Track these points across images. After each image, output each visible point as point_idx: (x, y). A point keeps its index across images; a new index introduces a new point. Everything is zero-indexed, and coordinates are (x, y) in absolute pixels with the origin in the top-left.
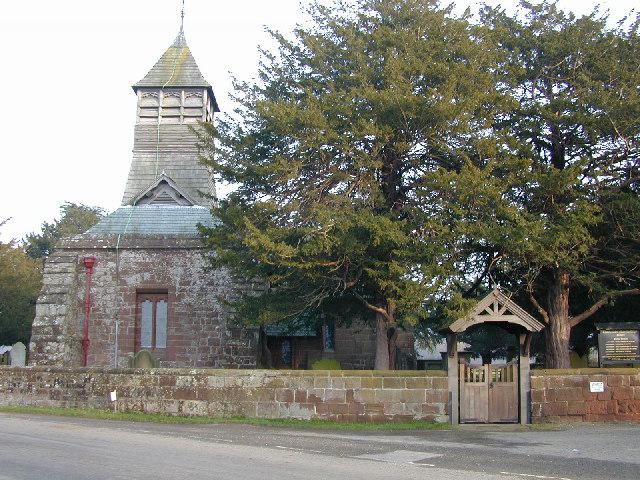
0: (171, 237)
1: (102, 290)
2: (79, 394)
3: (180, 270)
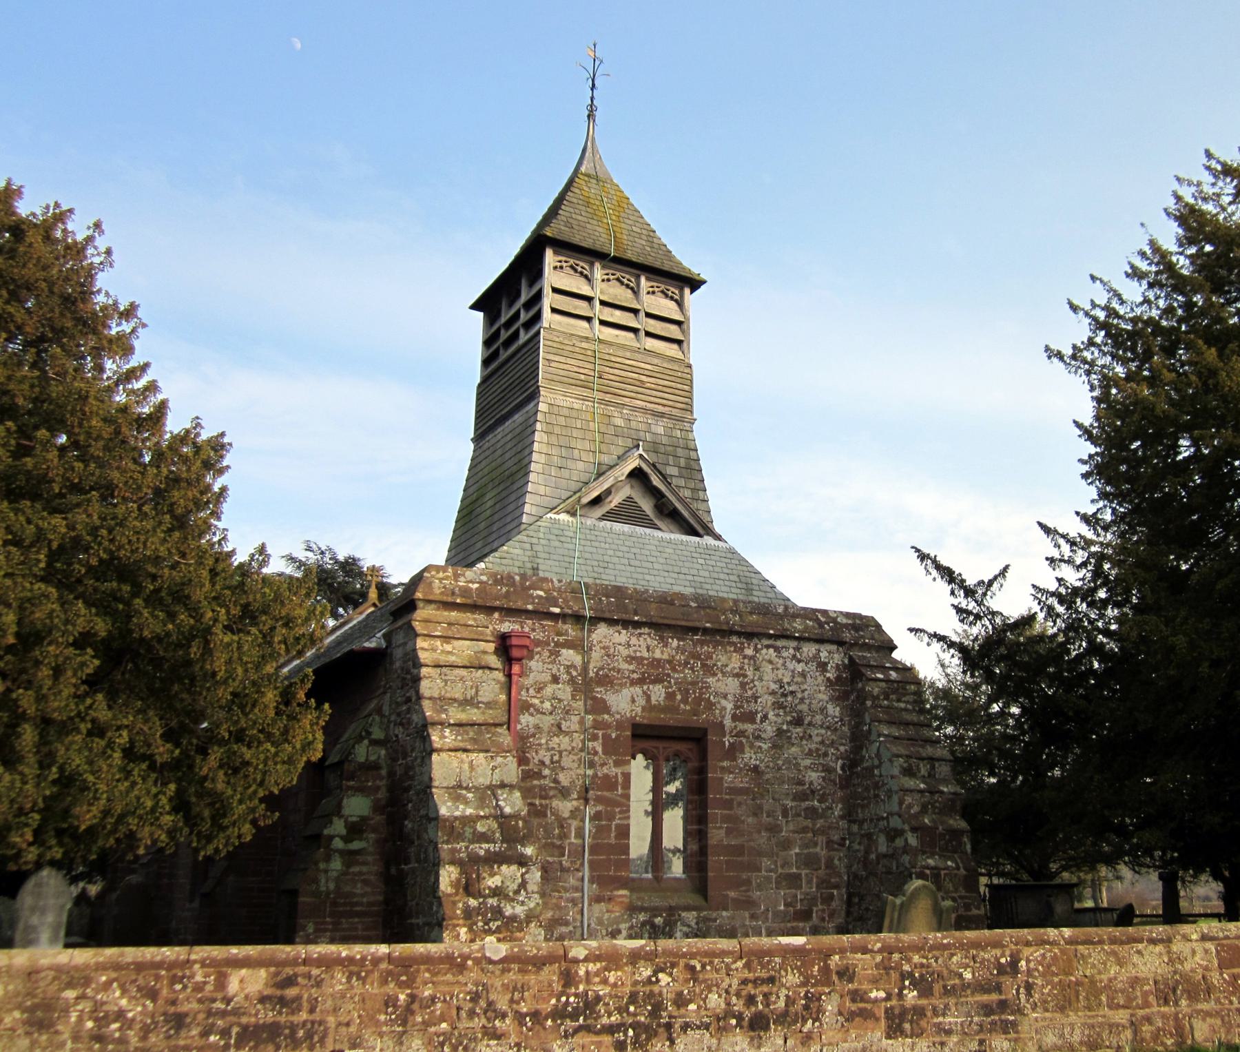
1: (547, 721)
2: (987, 1010)
3: (732, 685)
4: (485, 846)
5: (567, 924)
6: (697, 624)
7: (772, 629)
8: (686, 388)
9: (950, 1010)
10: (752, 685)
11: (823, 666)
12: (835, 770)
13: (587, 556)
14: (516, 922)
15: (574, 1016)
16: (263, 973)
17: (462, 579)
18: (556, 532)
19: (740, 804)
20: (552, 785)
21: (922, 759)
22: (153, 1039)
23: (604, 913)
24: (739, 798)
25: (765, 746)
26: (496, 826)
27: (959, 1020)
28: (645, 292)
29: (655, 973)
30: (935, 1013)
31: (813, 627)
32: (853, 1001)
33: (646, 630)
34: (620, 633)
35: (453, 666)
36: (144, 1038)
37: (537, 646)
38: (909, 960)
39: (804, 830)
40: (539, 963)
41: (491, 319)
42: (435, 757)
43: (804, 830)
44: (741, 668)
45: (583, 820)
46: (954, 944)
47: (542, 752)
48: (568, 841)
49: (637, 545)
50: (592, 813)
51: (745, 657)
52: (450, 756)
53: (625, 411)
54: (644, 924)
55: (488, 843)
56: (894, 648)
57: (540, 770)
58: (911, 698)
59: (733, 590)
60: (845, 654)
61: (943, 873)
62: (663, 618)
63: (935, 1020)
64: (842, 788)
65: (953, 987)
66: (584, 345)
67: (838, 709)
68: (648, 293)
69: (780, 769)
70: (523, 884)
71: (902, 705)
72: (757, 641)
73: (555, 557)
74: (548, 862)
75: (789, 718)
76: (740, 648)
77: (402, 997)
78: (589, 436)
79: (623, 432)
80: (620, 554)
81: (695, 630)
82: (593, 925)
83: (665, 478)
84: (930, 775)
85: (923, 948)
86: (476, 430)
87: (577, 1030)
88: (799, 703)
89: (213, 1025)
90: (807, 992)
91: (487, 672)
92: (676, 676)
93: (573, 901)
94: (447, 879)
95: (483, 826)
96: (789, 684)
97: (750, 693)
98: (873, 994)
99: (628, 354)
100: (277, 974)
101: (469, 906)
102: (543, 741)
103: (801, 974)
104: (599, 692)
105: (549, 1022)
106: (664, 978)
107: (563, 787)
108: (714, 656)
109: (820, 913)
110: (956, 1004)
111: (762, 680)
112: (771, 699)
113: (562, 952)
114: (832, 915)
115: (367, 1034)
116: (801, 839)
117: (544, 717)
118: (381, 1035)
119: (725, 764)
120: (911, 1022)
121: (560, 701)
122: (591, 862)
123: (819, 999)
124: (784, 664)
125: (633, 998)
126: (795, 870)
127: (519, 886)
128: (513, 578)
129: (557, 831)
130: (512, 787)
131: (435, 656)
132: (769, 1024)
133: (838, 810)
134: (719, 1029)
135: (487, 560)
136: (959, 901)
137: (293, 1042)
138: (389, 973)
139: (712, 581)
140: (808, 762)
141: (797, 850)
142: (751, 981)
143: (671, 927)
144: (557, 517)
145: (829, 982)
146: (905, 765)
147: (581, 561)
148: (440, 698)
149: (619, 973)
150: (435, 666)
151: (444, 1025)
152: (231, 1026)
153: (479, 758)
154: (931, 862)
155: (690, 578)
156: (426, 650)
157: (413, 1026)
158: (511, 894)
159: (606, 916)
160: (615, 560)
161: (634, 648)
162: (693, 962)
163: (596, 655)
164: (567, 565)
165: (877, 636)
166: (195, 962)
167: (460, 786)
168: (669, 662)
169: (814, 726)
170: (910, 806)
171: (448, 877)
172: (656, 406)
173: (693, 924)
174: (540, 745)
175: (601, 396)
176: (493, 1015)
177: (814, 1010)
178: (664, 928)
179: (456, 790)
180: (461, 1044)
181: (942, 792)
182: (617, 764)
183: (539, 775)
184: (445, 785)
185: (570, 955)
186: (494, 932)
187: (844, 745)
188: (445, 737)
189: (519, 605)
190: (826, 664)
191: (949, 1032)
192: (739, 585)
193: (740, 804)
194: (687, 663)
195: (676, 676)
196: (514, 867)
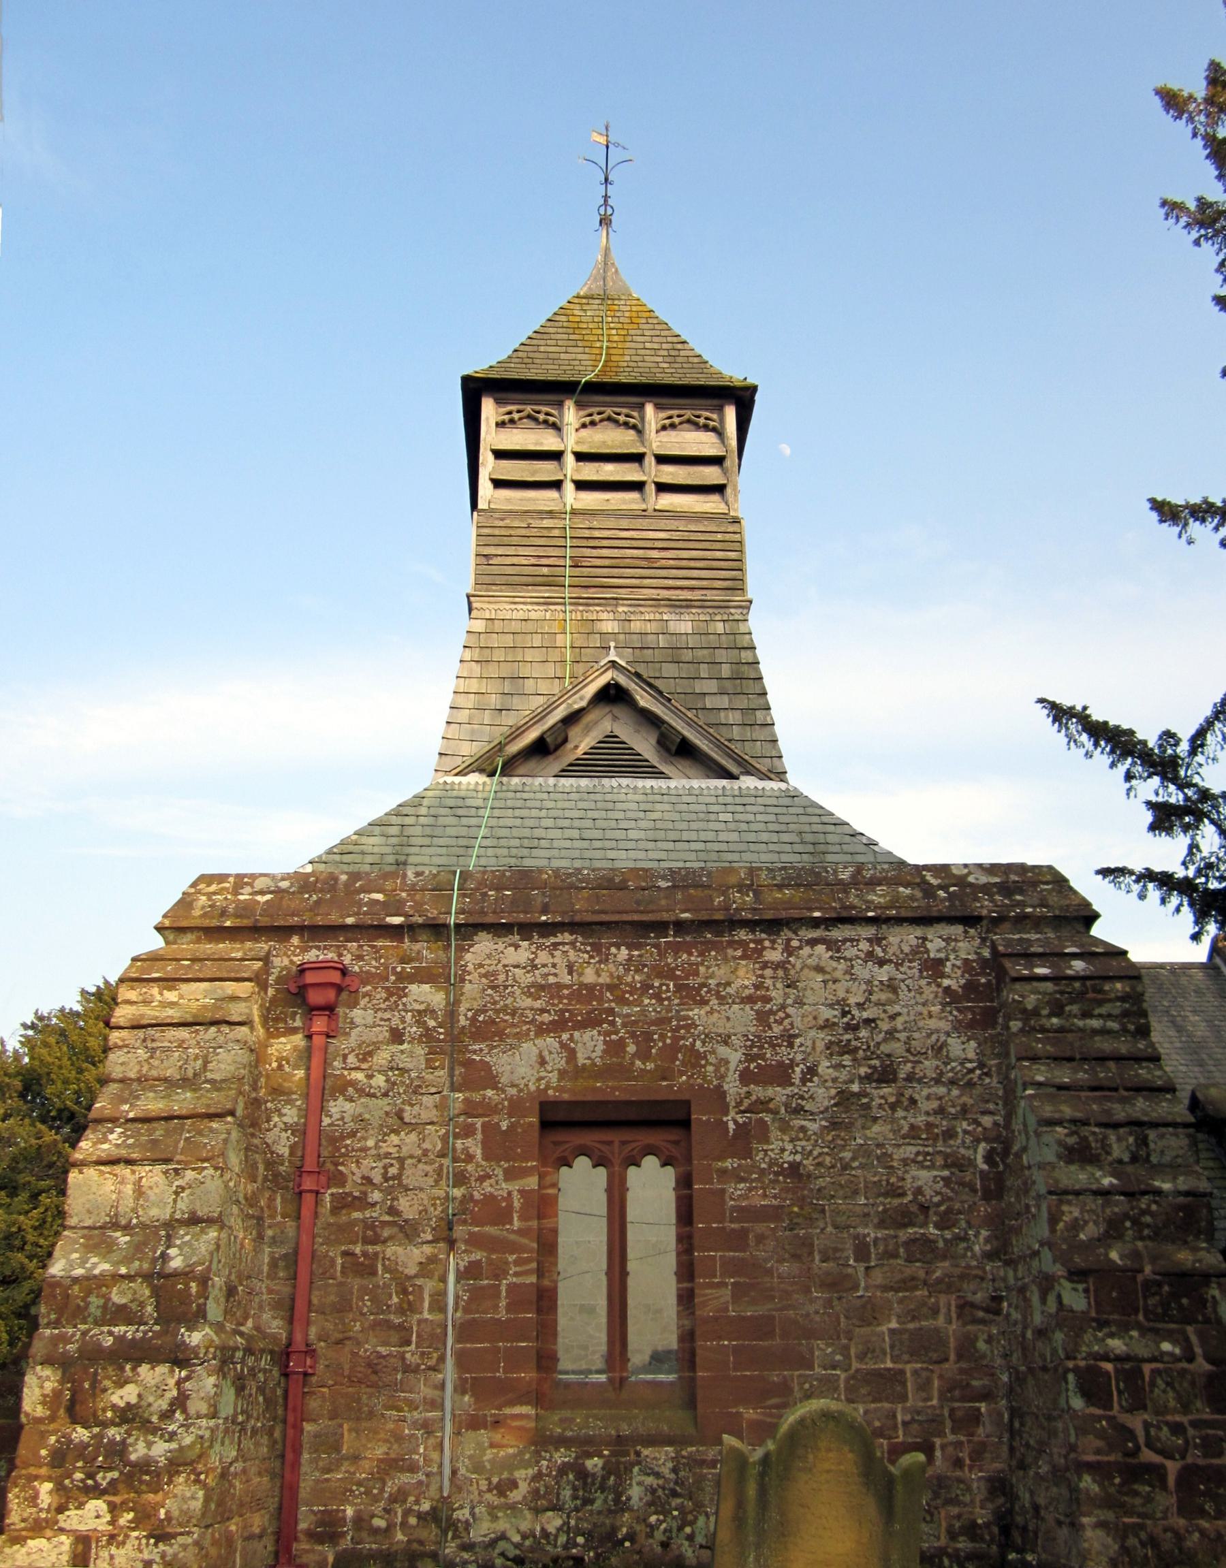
0: (684, 881)
3: (741, 1019)
5: (413, 1468)
6: (665, 916)
8: (732, 555)
10: (781, 1014)
11: (934, 968)
12: (972, 1163)
14: (147, 1473)
18: (451, 803)
19: (760, 1239)
20: (387, 1218)
21: (1116, 1126)
23: (483, 1451)
24: (760, 1228)
25: (813, 1127)
26: (147, 1292)
28: (654, 427)
33: (567, 937)
34: (517, 947)
39: (908, 1284)
42: (73, 1176)
43: (908, 1284)
44: (757, 987)
45: (443, 1279)
47: (367, 1163)
50: (462, 1264)
51: (765, 966)
52: (102, 1173)
53: (620, 609)
54: (563, 1470)
56: (1092, 917)
57: (365, 1194)
58: (1116, 1008)
60: (984, 940)
61: (1147, 1368)
62: (594, 912)
64: (987, 1196)
66: (547, 523)
67: (973, 1044)
69: (846, 1167)
70: (180, 1402)
71: (1095, 1023)
72: (791, 935)
75: (863, 1071)
76: (755, 950)
78: (555, 655)
81: (660, 927)
82: (463, 1471)
84: (1134, 1159)
88: (885, 1040)
92: (626, 1010)
93: (428, 1428)
95: (122, 1293)
96: (860, 1006)
97: (777, 1029)
99: (624, 523)
102: (370, 1143)
104: (478, 1051)
108: (702, 969)
109: (950, 1449)
111: (802, 1004)
112: (822, 1037)
114: (978, 1453)
116: (901, 1301)
117: (372, 1102)
119: (728, 1164)
121: (403, 1071)
124: (849, 972)
126: (889, 1365)
127: (171, 1404)
129: (395, 1300)
133: (980, 1242)
136: (1191, 1432)
140: (909, 1151)
141: (894, 1325)
146: (1072, 1140)
148: (139, 1080)
150: (133, 1027)
153: (153, 1176)
154: (1117, 1345)
155: (700, 846)
158: (155, 1419)
159: (489, 1454)
160: (557, 834)
161: (545, 970)
163: (471, 988)
164: (461, 851)
165: (1053, 899)
168: (611, 987)
169: (919, 1081)
170: (1075, 1226)
173: (666, 1471)
174: (365, 1149)
175: (577, 592)
178: (605, 1479)
181: (1158, 1192)
182: (510, 1175)
183: (362, 1202)
187: (991, 1113)
189: (334, 918)
190: (940, 962)
193: (760, 1239)
194: (646, 987)
196: (162, 1369)
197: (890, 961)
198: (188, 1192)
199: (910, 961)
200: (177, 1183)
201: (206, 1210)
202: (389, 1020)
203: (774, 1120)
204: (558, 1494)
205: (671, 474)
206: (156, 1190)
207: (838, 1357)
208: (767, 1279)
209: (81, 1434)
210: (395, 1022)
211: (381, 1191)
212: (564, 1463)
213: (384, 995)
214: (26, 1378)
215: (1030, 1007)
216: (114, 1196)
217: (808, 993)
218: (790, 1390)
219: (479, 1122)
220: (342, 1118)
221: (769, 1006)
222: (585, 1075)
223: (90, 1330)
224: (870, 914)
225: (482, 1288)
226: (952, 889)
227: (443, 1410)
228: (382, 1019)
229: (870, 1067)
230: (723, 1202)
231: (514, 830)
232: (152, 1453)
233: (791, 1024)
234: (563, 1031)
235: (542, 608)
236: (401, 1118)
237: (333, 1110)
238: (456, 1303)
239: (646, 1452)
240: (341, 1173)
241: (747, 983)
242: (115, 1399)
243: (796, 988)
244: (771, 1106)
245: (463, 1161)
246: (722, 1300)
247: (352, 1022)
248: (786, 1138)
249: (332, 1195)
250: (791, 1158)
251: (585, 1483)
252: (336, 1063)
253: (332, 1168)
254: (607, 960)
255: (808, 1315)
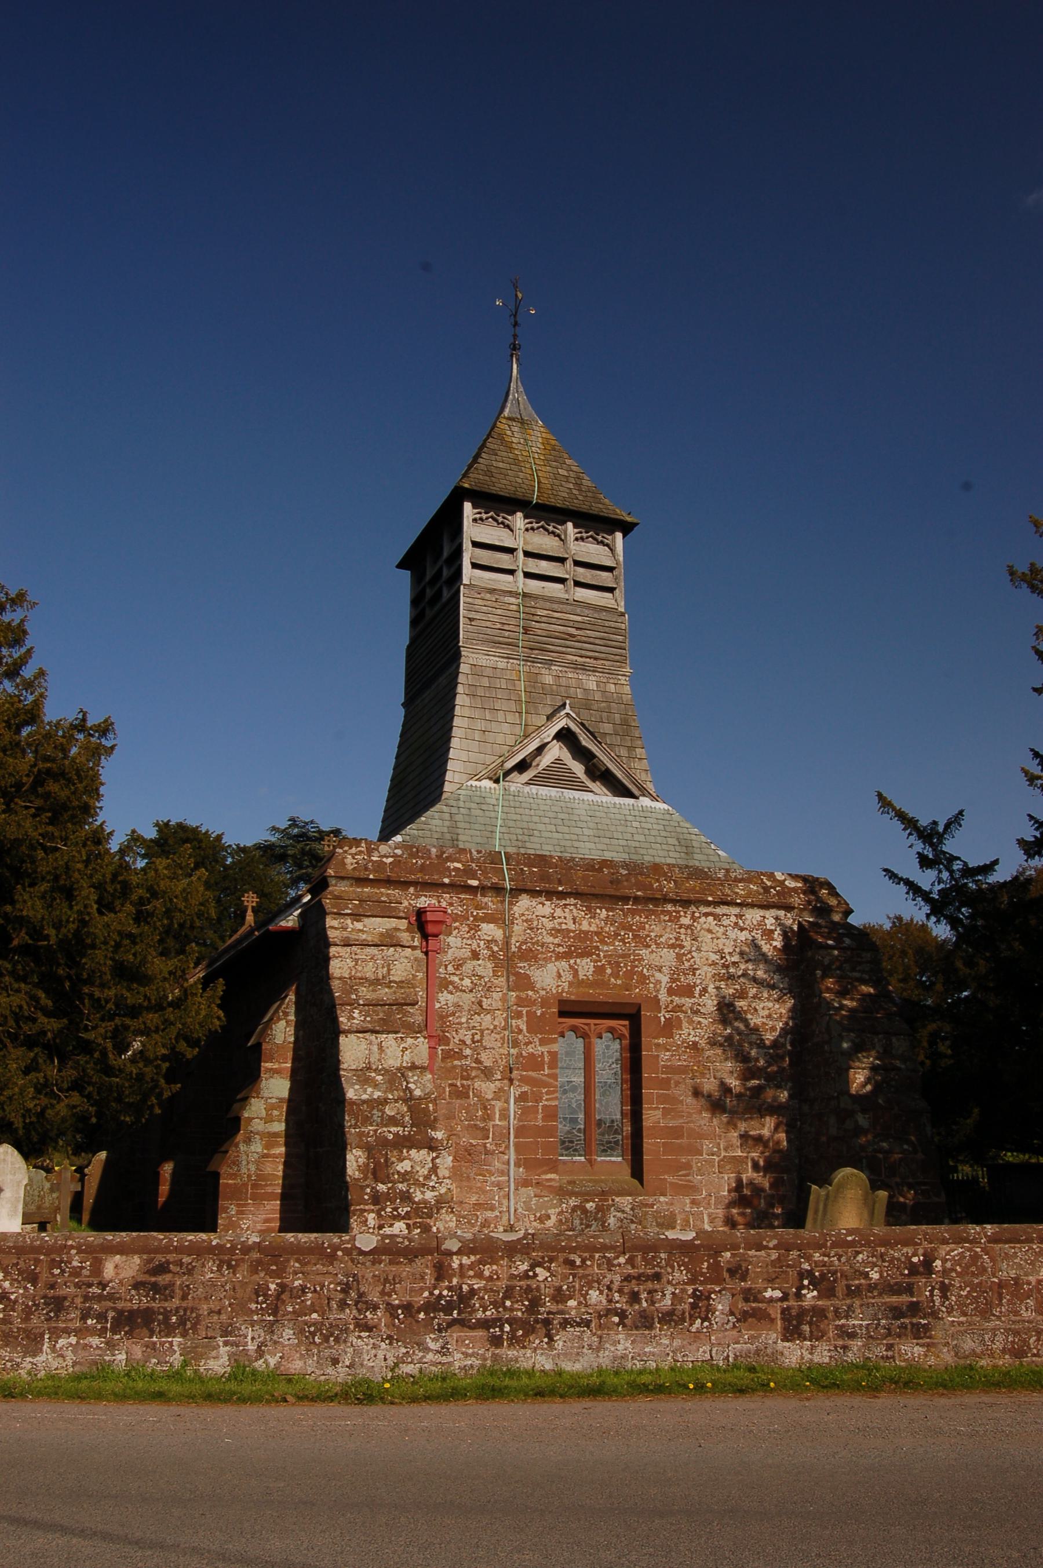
0: (634, 868)
1: (467, 999)
2: (896, 1312)
3: (668, 957)
4: (393, 1129)
5: (492, 1209)
7: (711, 895)
9: (854, 1312)
10: (689, 956)
13: (512, 823)
15: (448, 1309)
16: (137, 1260)
17: (376, 853)
20: (474, 1065)
22: (34, 1320)
24: (676, 1077)
26: (405, 1109)
27: (864, 1323)
28: (573, 538)
29: (532, 1267)
30: (837, 1315)
31: (757, 891)
32: (746, 1300)
33: (573, 901)
34: (544, 905)
35: (365, 944)
36: (27, 1319)
37: (455, 921)
38: (808, 1258)
40: (411, 1254)
41: (417, 579)
44: (677, 939)
45: (507, 1101)
46: (859, 1242)
48: (492, 1123)
49: (565, 810)
50: (517, 1093)
52: (359, 1038)
53: (553, 668)
54: (574, 1209)
55: (396, 1126)
57: (461, 1050)
59: (671, 854)
63: (837, 1323)
65: (858, 1287)
68: (577, 539)
70: (434, 1169)
72: (695, 909)
73: (477, 826)
74: (472, 1145)
77: (273, 1286)
79: (552, 690)
80: (547, 820)
82: (520, 1210)
83: (595, 738)
85: (824, 1246)
86: (406, 694)
87: (451, 1324)
89: (90, 1308)
90: (695, 1290)
91: (399, 949)
92: (605, 948)
94: (355, 1164)
95: (391, 1109)
97: (687, 964)
98: (768, 1294)
100: (150, 1261)
101: (378, 1191)
102: (464, 1020)
103: (688, 1271)
104: (522, 967)
105: (422, 1315)
106: (542, 1273)
107: (485, 1067)
108: (647, 926)
110: (861, 1305)
112: (710, 971)
113: (435, 1244)
115: (238, 1322)
118: (253, 1324)
119: (660, 1041)
120: (810, 1323)
121: (481, 977)
122: (516, 1145)
123: (709, 1298)
125: (509, 1293)
128: (429, 851)
129: (480, 1113)
130: (423, 1069)
131: (345, 934)
132: (654, 1323)
134: (600, 1326)
135: (403, 832)
137: (166, 1328)
138: (259, 1262)
139: (647, 845)
142: (634, 1278)
143: (603, 1212)
144: (478, 783)
145: (719, 1281)
146: (857, 1041)
147: (504, 830)
149: (495, 1267)
151: (315, 1316)
152: (107, 1311)
155: (624, 843)
156: (336, 929)
157: (284, 1315)
158: (421, 1179)
159: (534, 1201)
161: (560, 920)
162: (572, 1257)
163: (518, 928)
164: (489, 834)
166: (72, 1247)
167: (369, 1068)
168: (597, 934)
169: (759, 999)
171: (355, 1160)
172: (588, 660)
173: (627, 1209)
176: (364, 1306)
177: (703, 1309)
178: (597, 1213)
179: (363, 1076)
180: (332, 1335)
182: (543, 1042)
183: (460, 1056)
184: (354, 1067)
185: (443, 1247)
186: (403, 1218)
188: (354, 1018)
191: (852, 1336)
192: (678, 849)
193: (677, 1083)
194: (617, 935)
195: (605, 948)
196: (424, 1152)
197: (747, 929)
198: (409, 1050)
199: (757, 930)
200: (402, 1046)
201: (420, 1062)
202: (470, 945)
203: (685, 1017)
204: (572, 1222)
205: (584, 575)
206: (391, 1049)
207: (715, 1149)
208: (680, 1106)
209: (382, 1187)
210: (474, 946)
211: (471, 1049)
212: (575, 1206)
213: (467, 929)
214: (348, 1157)
215: (826, 963)
216: (367, 1052)
217: (704, 944)
218: (691, 1167)
219: (524, 1011)
220: (447, 1004)
221: (683, 951)
222: (584, 985)
223: (377, 1130)
224: (738, 901)
225: (528, 1107)
226: (778, 889)
227: (509, 1176)
228: (466, 944)
229: (735, 989)
230: (658, 1063)
231: (518, 823)
232: (426, 1198)
233: (695, 962)
234: (571, 958)
235: (505, 660)
236: (481, 1006)
237: (441, 999)
238: (515, 1116)
239: (617, 1199)
240: (447, 1037)
241: (671, 936)
242: (399, 1168)
243: (697, 941)
244: (684, 1009)
245: (517, 1033)
246: (657, 1117)
247: (449, 945)
248: (691, 1028)
249: (442, 1050)
250: (693, 1039)
251: (586, 1216)
252: (441, 970)
253: (441, 1034)
254: (595, 917)
255: (700, 1126)
